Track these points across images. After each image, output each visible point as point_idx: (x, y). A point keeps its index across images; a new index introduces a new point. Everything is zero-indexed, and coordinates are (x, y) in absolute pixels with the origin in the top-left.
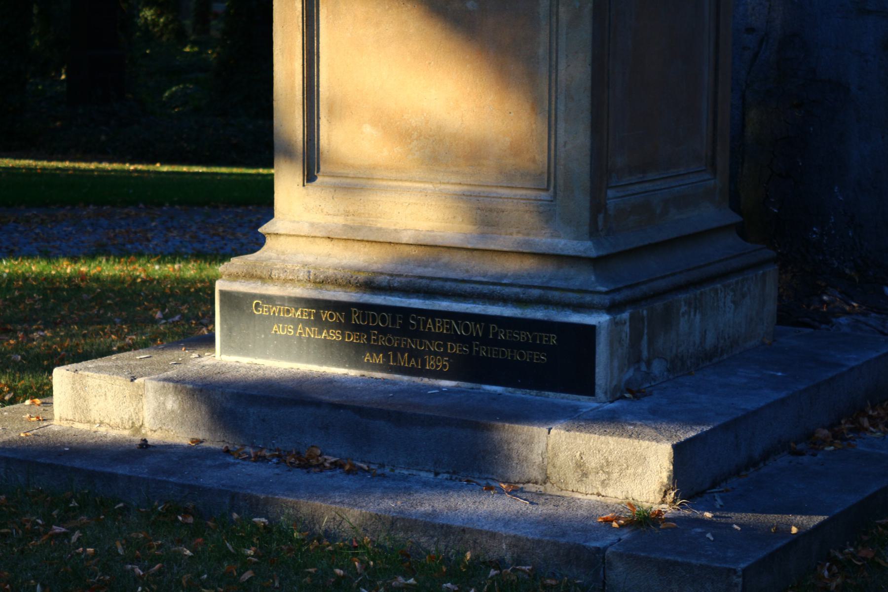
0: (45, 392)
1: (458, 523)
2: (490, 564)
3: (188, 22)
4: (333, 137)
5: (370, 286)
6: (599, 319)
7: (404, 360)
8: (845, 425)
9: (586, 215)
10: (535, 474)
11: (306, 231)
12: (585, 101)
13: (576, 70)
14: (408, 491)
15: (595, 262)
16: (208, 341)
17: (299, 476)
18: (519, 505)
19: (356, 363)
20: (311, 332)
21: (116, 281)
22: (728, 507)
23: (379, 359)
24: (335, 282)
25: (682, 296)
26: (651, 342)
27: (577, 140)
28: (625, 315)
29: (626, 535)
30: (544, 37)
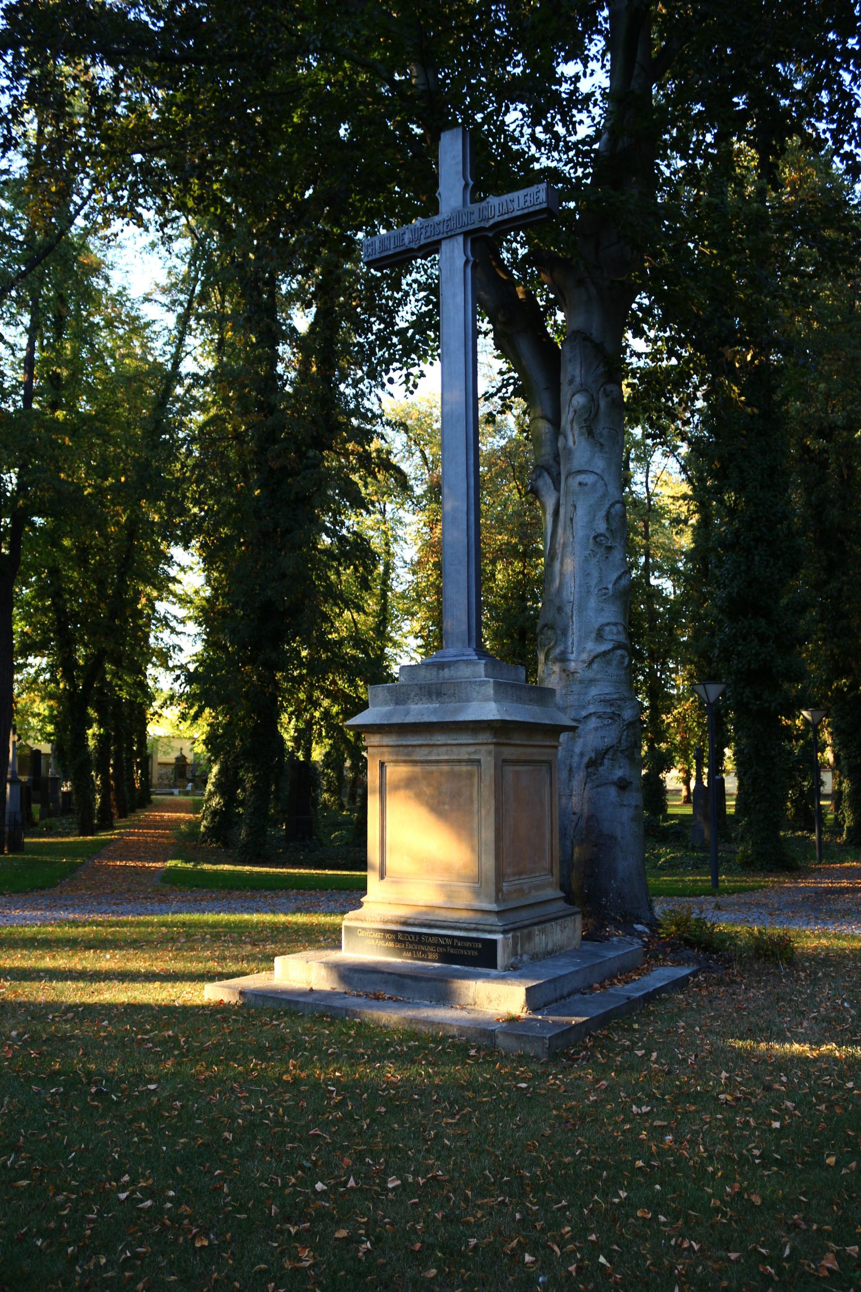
0: (271, 969)
1: (437, 1020)
2: (450, 1037)
3: (345, 799)
4: (391, 862)
5: (405, 923)
6: (498, 937)
7: (419, 955)
8: (607, 982)
9: (494, 894)
10: (471, 1001)
11: (385, 900)
12: (493, 847)
13: (488, 834)
14: (418, 1008)
15: (498, 913)
16: (339, 947)
17: (374, 1002)
18: (464, 1014)
19: (400, 956)
20: (382, 943)
21: (304, 924)
22: (548, 1014)
23: (409, 954)
24: (392, 922)
25: (536, 928)
26: (522, 947)
27: (489, 863)
28: (510, 935)
29: (504, 1025)
30: (476, 820)
